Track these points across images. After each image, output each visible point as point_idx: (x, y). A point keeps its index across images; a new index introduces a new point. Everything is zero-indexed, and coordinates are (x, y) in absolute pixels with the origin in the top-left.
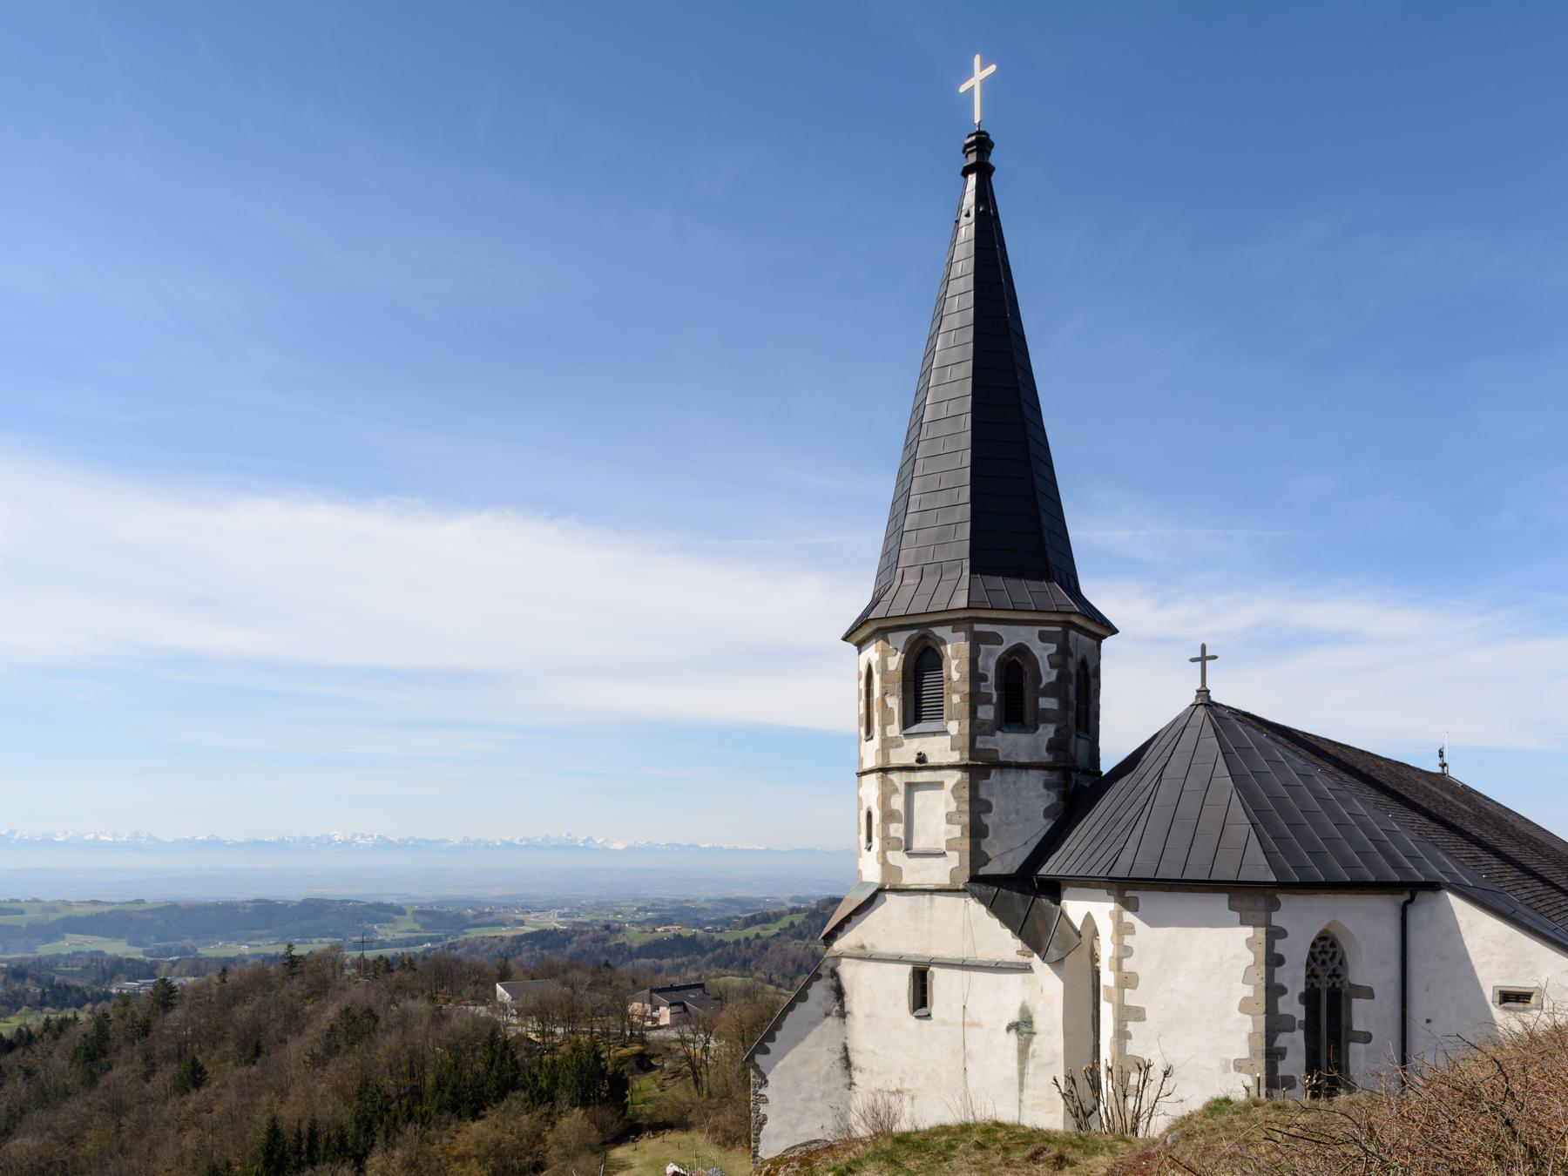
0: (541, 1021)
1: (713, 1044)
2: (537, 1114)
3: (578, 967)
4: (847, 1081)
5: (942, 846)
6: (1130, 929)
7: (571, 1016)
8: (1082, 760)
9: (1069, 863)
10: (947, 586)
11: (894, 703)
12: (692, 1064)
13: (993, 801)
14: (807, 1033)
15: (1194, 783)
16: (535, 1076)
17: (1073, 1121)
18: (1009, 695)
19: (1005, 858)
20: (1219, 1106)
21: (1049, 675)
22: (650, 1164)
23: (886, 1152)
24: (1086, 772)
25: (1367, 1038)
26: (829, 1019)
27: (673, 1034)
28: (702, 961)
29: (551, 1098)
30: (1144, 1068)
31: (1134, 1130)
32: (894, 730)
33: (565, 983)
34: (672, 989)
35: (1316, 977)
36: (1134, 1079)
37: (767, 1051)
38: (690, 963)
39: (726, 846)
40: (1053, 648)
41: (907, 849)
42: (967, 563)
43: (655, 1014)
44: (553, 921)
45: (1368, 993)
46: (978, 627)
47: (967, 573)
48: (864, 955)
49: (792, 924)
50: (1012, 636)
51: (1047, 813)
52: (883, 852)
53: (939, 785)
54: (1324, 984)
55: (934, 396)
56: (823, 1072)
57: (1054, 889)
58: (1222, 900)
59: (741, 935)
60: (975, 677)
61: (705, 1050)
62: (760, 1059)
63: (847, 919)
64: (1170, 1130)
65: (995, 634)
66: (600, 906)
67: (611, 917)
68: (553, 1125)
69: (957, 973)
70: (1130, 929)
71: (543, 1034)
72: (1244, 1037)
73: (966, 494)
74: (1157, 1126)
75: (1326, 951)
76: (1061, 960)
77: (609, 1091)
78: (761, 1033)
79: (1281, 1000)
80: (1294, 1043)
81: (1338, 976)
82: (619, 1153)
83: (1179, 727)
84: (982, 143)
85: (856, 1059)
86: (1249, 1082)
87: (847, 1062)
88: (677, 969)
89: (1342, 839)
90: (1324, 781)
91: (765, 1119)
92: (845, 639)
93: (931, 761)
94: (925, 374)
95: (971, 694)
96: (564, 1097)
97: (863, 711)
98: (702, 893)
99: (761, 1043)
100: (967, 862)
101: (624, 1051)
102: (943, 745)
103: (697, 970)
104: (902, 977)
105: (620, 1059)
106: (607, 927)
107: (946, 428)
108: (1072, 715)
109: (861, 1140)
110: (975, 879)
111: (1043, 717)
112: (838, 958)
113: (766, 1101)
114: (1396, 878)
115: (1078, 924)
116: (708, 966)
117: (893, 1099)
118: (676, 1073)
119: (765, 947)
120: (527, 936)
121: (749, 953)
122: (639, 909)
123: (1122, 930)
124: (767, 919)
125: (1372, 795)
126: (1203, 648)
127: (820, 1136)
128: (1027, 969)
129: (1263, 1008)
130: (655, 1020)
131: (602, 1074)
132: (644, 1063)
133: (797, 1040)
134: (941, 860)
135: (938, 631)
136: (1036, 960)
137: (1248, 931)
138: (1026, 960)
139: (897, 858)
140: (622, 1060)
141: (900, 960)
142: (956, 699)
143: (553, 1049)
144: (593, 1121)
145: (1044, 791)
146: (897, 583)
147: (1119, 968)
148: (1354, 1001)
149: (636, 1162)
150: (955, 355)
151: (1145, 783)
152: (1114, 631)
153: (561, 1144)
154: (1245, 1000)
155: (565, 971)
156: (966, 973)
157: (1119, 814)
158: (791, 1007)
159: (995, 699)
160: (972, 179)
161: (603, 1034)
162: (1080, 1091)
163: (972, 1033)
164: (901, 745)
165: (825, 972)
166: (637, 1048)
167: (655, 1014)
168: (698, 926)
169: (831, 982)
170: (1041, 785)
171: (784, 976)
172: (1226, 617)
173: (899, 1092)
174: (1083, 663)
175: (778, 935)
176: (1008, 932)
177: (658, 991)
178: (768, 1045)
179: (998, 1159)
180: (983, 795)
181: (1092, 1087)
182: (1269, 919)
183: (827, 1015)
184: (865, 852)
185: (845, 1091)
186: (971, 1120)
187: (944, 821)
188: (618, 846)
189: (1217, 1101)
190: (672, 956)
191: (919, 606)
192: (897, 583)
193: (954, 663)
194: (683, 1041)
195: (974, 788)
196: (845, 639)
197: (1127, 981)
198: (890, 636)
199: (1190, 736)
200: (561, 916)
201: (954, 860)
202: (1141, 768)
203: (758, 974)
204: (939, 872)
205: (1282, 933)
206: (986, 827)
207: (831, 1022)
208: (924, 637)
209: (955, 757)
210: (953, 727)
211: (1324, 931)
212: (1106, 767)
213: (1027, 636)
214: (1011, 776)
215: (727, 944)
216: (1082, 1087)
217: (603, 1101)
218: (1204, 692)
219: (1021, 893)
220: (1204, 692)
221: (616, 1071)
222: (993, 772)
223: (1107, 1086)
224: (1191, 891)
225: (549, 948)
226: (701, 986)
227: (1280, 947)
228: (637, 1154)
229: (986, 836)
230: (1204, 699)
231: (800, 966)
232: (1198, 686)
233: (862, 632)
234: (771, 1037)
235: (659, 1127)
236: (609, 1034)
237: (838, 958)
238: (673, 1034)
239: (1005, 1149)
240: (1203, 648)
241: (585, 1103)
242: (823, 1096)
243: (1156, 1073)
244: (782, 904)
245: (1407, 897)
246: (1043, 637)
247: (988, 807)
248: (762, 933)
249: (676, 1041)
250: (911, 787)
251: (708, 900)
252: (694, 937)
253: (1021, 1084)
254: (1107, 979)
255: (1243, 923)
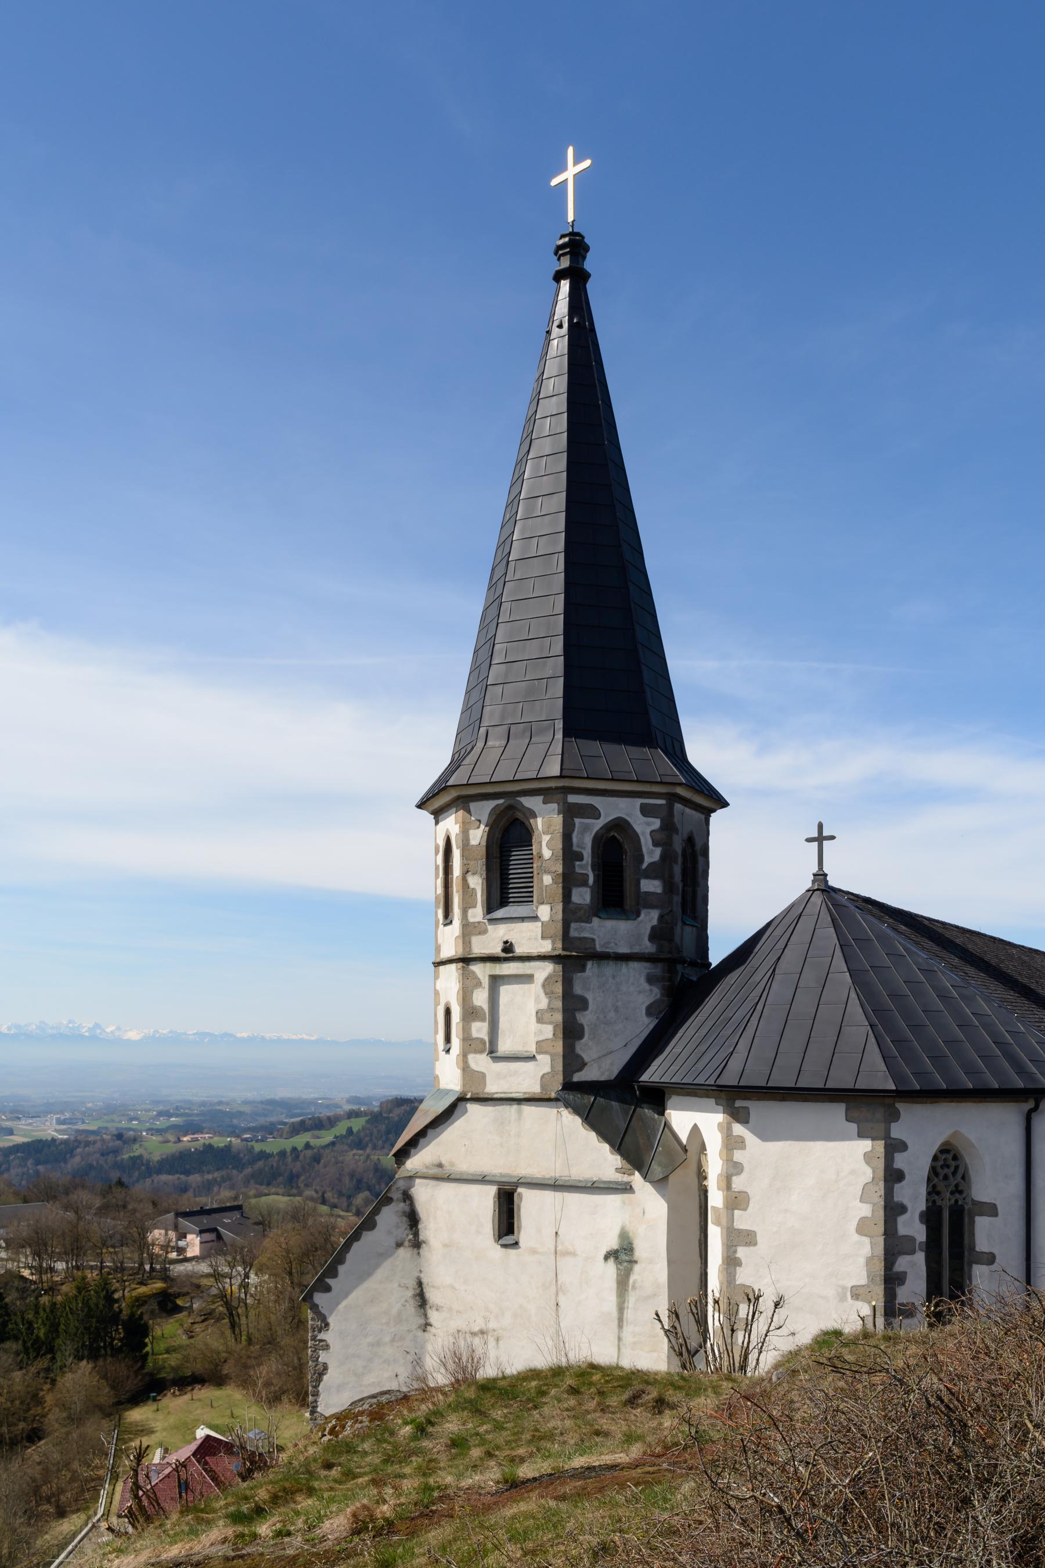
0: (37, 1254)
1: (253, 1279)
2: (33, 1369)
3: (83, 1187)
4: (422, 1321)
5: (532, 1049)
6: (741, 1143)
7: (75, 1248)
8: (689, 951)
9: (674, 1068)
10: (537, 750)
11: (477, 883)
12: (227, 1304)
13: (590, 997)
14: (377, 1266)
15: (810, 978)
16: (30, 1323)
17: (676, 1362)
18: (608, 876)
19: (603, 1064)
20: (830, 1338)
21: (652, 854)
22: (176, 1428)
23: (470, 1401)
24: (693, 964)
25: (990, 1259)
26: (401, 1251)
27: (204, 1268)
28: (239, 1177)
29: (51, 1350)
30: (753, 1299)
31: (743, 1367)
32: (477, 914)
33: (66, 1208)
34: (203, 1212)
35: (938, 1193)
36: (744, 1310)
37: (328, 1289)
38: (224, 1180)
39: (268, 1036)
40: (656, 823)
41: (491, 1052)
42: (559, 725)
43: (181, 1243)
44: (50, 1129)
45: (991, 1210)
46: (572, 799)
47: (559, 735)
48: (442, 1176)
49: (350, 1131)
50: (611, 809)
51: (649, 1011)
52: (464, 1055)
53: (528, 978)
54: (946, 1201)
55: (522, 531)
56: (394, 1311)
57: (657, 1098)
58: (838, 1111)
59: (287, 1144)
60: (569, 854)
61: (244, 1286)
62: (319, 1298)
63: (422, 1134)
64: (776, 1366)
65: (591, 807)
66: (110, 1109)
67: (124, 1124)
68: (53, 1382)
69: (548, 1195)
70: (741, 1143)
71: (39, 1270)
72: (862, 1261)
73: (558, 646)
74: (765, 1362)
75: (949, 1166)
76: (665, 1178)
77: (123, 1344)
78: (317, 1268)
79: (901, 1220)
80: (915, 1266)
81: (961, 1192)
82: (136, 1415)
83: (793, 915)
84: (575, 246)
85: (431, 1295)
86: (866, 1310)
87: (421, 1300)
88: (207, 1187)
89: (965, 1036)
90: (948, 976)
91: (325, 1367)
92: (421, 805)
93: (519, 950)
94: (513, 503)
95: (564, 875)
96: (66, 1348)
97: (440, 891)
98: (239, 1094)
99: (320, 1280)
100: (560, 1068)
101: (143, 1290)
102: (533, 932)
103: (232, 1187)
104: (486, 1198)
105: (137, 1299)
106: (120, 1136)
107: (536, 568)
108: (677, 899)
109: (439, 1390)
110: (569, 1086)
111: (645, 901)
112: (411, 1178)
113: (327, 1347)
114: (1020, 1084)
115: (684, 1138)
116: (247, 1182)
117: (477, 1341)
118: (207, 1316)
119: (317, 1159)
120: (17, 1148)
121: (297, 1167)
122: (160, 1114)
123: (732, 1144)
124: (319, 1124)
125: (999, 991)
126: (820, 826)
127: (393, 1386)
128: (627, 1188)
129: (881, 1228)
130: (181, 1250)
131: (115, 1318)
132: (167, 1304)
133: (365, 1275)
134: (530, 1065)
135: (528, 802)
136: (637, 1178)
137: (866, 1145)
138: (626, 1178)
139: (480, 1062)
140: (140, 1301)
141: (482, 1180)
142: (547, 880)
143: (52, 1289)
144: (105, 1377)
145: (647, 987)
146: (480, 744)
147: (729, 1187)
148: (978, 1219)
149: (158, 1426)
150: (546, 485)
151: (757, 978)
152: (724, 804)
153: (63, 1406)
154: (863, 1220)
155: (67, 1193)
156: (559, 1195)
157: (729, 1013)
158: (356, 1236)
159: (591, 881)
160: (565, 286)
161: (116, 1270)
162: (685, 1327)
163: (564, 1263)
164: (485, 932)
165: (396, 1195)
166: (159, 1285)
167: (181, 1243)
168: (233, 1134)
169: (402, 1206)
170: (642, 980)
171: (340, 1194)
172: (855, 762)
173: (482, 1332)
174: (690, 841)
175: (333, 1144)
176: (606, 1147)
177: (186, 1215)
178: (329, 1281)
179: (592, 1405)
180: (578, 990)
181: (697, 1322)
182: (888, 1131)
183: (399, 1245)
184: (442, 1054)
185: (420, 1333)
186: (564, 1363)
187: (534, 1019)
188: (133, 1035)
189: (826, 1333)
190: (200, 1171)
191: (504, 773)
192: (480, 744)
193: (546, 838)
194: (217, 1276)
195: (567, 983)
196: (421, 805)
197: (736, 1201)
198: (473, 806)
199: (805, 926)
200: (60, 1122)
201: (544, 1064)
202: (754, 961)
203: (309, 1193)
204: (528, 1078)
205: (902, 1146)
206: (582, 1026)
207: (404, 1253)
208: (511, 808)
209: (546, 947)
210: (544, 912)
211: (946, 1143)
212: (716, 956)
213: (628, 809)
214: (609, 969)
215: (270, 1155)
216: (687, 1322)
217: (116, 1352)
218: (820, 876)
219: (621, 1103)
220: (820, 876)
221: (132, 1315)
222: (589, 964)
223: (714, 1320)
224: (806, 1100)
225: (45, 1163)
226: (239, 1208)
227: (900, 1161)
228: (160, 1416)
229: (581, 1036)
230: (821, 884)
231: (359, 1181)
232: (815, 869)
233: (438, 800)
234: (332, 1272)
235: (187, 1382)
236: (122, 1269)
237: (411, 1178)
238: (204, 1268)
239: (601, 1393)
240: (820, 826)
241: (93, 1355)
242: (393, 1340)
243: (766, 1304)
244: (337, 1106)
245: (1031, 1104)
246: (645, 811)
247: (583, 1004)
248: (314, 1142)
249: (208, 1275)
250: (496, 981)
251: (246, 1102)
252: (229, 1147)
253: (620, 1320)
254: (716, 1199)
255: (861, 1135)
